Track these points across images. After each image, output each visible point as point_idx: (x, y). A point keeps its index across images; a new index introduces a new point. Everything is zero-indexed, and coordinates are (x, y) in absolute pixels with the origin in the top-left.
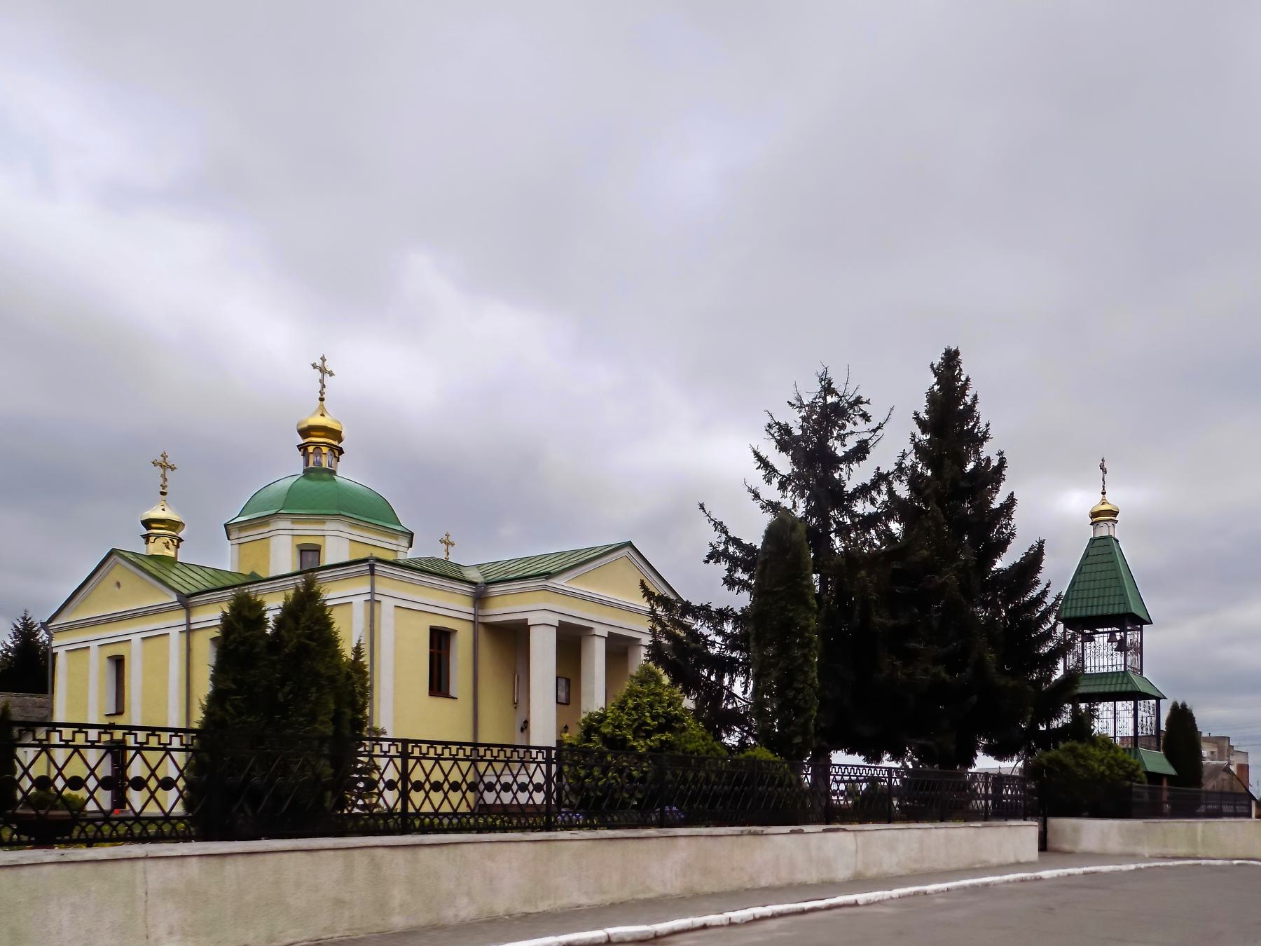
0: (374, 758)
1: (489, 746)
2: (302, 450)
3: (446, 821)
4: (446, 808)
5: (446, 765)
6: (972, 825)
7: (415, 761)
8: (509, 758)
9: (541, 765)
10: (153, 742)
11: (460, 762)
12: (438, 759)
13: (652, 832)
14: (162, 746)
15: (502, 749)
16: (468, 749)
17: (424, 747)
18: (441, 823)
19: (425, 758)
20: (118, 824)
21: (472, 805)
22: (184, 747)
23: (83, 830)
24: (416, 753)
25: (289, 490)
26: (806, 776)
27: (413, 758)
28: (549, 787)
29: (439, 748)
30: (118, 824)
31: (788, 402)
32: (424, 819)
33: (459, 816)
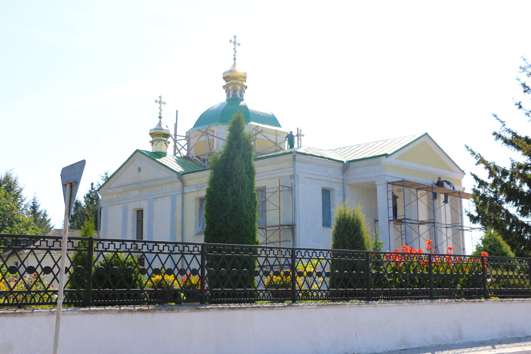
2: (226, 88)
3: (315, 294)
5: (189, 258)
9: (289, 259)
12: (170, 254)
16: (171, 246)
17: (161, 246)
19: (161, 253)
20: (35, 294)
21: (182, 285)
23: (15, 297)
25: (222, 112)
27: (298, 258)
28: (203, 272)
29: (118, 244)
30: (35, 294)
31: (177, 111)
32: (313, 292)
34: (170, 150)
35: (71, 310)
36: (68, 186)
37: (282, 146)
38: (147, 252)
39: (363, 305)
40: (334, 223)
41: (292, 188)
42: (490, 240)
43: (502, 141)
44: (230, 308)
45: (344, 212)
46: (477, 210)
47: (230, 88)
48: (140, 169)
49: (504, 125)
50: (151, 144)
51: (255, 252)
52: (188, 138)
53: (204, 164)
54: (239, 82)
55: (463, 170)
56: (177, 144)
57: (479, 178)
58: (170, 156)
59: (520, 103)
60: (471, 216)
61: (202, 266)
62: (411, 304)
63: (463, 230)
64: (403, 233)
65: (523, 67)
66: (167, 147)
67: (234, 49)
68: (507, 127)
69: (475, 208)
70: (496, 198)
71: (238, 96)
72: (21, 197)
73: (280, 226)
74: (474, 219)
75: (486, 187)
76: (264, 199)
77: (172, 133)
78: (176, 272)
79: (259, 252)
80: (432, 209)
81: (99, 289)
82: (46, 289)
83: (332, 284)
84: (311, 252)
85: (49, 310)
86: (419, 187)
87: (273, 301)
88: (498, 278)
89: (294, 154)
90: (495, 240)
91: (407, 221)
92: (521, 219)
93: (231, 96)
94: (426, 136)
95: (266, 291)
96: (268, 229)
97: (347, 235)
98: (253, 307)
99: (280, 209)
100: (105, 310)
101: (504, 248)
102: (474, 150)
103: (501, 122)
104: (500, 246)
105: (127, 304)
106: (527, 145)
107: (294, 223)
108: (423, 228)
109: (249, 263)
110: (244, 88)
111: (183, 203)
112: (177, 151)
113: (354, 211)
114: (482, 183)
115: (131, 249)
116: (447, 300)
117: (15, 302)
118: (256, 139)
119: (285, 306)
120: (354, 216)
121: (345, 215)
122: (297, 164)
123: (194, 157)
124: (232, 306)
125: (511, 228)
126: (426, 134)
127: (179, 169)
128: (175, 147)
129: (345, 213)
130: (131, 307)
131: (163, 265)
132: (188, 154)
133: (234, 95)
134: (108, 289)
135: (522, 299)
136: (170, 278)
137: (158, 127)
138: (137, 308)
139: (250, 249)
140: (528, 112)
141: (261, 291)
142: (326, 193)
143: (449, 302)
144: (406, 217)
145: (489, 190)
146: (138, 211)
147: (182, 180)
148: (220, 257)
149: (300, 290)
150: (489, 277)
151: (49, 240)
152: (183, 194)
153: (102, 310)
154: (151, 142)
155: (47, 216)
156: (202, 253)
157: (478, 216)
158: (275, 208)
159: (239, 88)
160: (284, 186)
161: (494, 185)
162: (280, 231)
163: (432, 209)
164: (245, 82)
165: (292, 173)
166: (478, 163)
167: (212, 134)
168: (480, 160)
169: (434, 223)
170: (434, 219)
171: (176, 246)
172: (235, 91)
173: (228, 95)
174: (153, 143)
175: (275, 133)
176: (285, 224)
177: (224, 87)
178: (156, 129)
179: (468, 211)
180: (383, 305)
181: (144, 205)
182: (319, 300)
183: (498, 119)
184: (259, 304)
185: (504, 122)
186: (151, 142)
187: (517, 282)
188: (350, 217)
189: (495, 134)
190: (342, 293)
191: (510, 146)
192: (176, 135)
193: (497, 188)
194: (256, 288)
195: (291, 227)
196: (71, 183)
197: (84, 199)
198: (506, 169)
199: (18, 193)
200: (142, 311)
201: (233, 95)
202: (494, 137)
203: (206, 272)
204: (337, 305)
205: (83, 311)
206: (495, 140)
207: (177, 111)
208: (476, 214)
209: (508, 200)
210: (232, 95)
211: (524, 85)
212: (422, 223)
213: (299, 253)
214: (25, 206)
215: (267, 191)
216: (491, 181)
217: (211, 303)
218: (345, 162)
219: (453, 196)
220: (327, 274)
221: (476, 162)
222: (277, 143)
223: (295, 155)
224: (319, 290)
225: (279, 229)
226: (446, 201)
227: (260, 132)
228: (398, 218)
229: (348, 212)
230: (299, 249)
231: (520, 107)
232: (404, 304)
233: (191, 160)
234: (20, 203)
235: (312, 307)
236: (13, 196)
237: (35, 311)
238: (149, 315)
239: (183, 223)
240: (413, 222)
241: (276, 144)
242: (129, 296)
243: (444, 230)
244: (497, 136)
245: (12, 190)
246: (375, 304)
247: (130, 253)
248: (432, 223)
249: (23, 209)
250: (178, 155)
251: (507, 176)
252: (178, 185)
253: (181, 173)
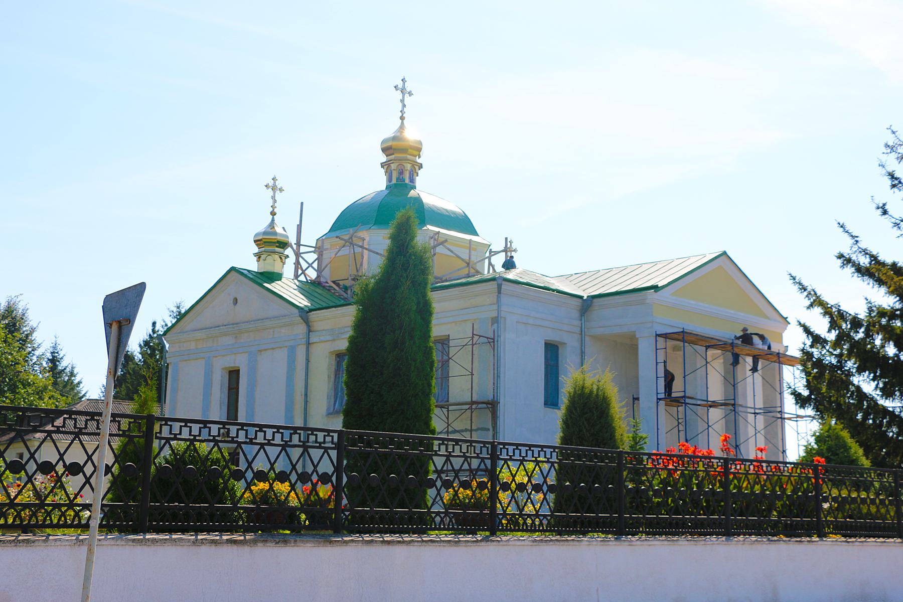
0: (309, 449)
2: (386, 167)
3: (529, 521)
8: (286, 442)
10: (205, 435)
11: (310, 450)
12: (285, 446)
15: (751, 463)
17: (269, 432)
18: (525, 523)
22: (302, 444)
24: (165, 432)
25: (379, 207)
27: (502, 459)
28: (339, 479)
29: (195, 428)
31: (302, 203)
34: (288, 270)
35: (113, 539)
36: (115, 327)
37: (478, 268)
38: (245, 443)
39: (610, 543)
40: (564, 401)
41: (494, 339)
42: (829, 436)
43: (853, 269)
44: (383, 542)
45: (581, 383)
46: (808, 386)
47: (393, 166)
48: (236, 301)
49: (857, 241)
50: (255, 258)
51: (429, 447)
52: (319, 249)
53: (345, 295)
54: (409, 157)
55: (785, 317)
56: (301, 260)
57: (812, 330)
58: (287, 279)
59: (884, 205)
60: (797, 396)
61: (338, 469)
62: (692, 543)
63: (783, 419)
64: (680, 421)
65: (891, 144)
66: (284, 263)
67: (402, 101)
68: (863, 245)
69: (804, 382)
70: (840, 366)
71: (407, 181)
72: (31, 342)
73: (473, 403)
74: (801, 401)
75: (824, 347)
76: (445, 358)
77: (293, 240)
78: (294, 477)
79: (436, 448)
80: (732, 383)
81: (162, 504)
83: (559, 506)
84: (523, 449)
85: (74, 538)
86: (710, 343)
87: (457, 532)
88: (842, 503)
89: (500, 281)
90: (838, 437)
91: (688, 401)
92: (882, 402)
93: (394, 181)
94: (724, 257)
95: (446, 514)
96: (451, 408)
97: (585, 423)
98: (423, 541)
99: (472, 375)
100: (171, 540)
101: (853, 451)
102: (805, 283)
103: (852, 236)
104: (846, 448)
105: (209, 530)
106: (895, 276)
107: (496, 399)
108: (716, 414)
109: (419, 465)
110: (417, 168)
111: (308, 361)
112: (300, 272)
113: (599, 381)
114: (817, 340)
116: (753, 538)
118: (435, 254)
119: (477, 541)
120: (598, 389)
121: (583, 387)
122: (504, 299)
123: (329, 282)
124: (388, 537)
125: (865, 418)
126: (725, 253)
127: (302, 301)
128: (297, 264)
129: (584, 384)
130: (214, 536)
131: (272, 465)
132: (318, 276)
133: (400, 179)
134: (177, 504)
135: (881, 540)
136: (282, 488)
137: (269, 230)
138: (225, 538)
139: (421, 441)
140: (898, 222)
141: (438, 513)
142: (552, 350)
143: (756, 540)
144: (687, 395)
145: (828, 351)
146: (231, 372)
147: (307, 322)
148: (369, 453)
149: (505, 514)
150: (826, 500)
152: (309, 344)
153: (166, 539)
154: (255, 255)
155: (75, 376)
156: (338, 447)
157: (809, 396)
158: (464, 372)
159: (408, 166)
160: (480, 336)
161: (837, 343)
162: (472, 412)
163: (732, 383)
164: (419, 157)
165: (495, 314)
166: (811, 305)
167: (361, 244)
168: (815, 301)
169: (734, 405)
170: (734, 399)
172: (401, 173)
173: (390, 179)
174: (260, 257)
175: (468, 245)
176: (479, 400)
177: (383, 165)
178: (265, 233)
179: (793, 387)
180: (645, 543)
181: (241, 362)
182: (535, 531)
183: (847, 232)
184: (433, 535)
185: (857, 237)
186: (255, 255)
187: (873, 509)
188: (591, 392)
189: (841, 256)
190: (575, 521)
191: (866, 278)
192: (298, 244)
193: (842, 349)
194: (429, 509)
195: (490, 406)
196: (119, 322)
197: (139, 349)
198: (859, 316)
199: (27, 336)
200: (229, 541)
201: (398, 179)
202: (840, 262)
203: (345, 479)
204: (567, 540)
205: (134, 540)
206: (841, 267)
207: (302, 203)
208: (805, 393)
209: (860, 370)
210: (397, 179)
211: (892, 176)
212: (714, 405)
213: (505, 451)
214: (40, 358)
215: (451, 343)
216: (832, 336)
217: (351, 532)
218: (585, 298)
219: (768, 360)
220: (551, 489)
221: (808, 303)
222: (471, 264)
223: (501, 284)
224: (537, 515)
225: (471, 408)
226: (754, 369)
227: (442, 243)
228: (674, 395)
229: (588, 383)
230: (504, 444)
231: (885, 212)
232: (680, 543)
233: (324, 287)
234: (30, 353)
235: (523, 543)
236: (18, 341)
237: (51, 538)
238: (246, 549)
239: (306, 395)
240: (699, 402)
241: (468, 264)
242: (212, 518)
243: (751, 417)
244: (845, 260)
245: (18, 330)
246: (632, 541)
248: (731, 405)
249: (34, 364)
250: (302, 278)
251: (860, 328)
252: (301, 328)
253: (307, 309)
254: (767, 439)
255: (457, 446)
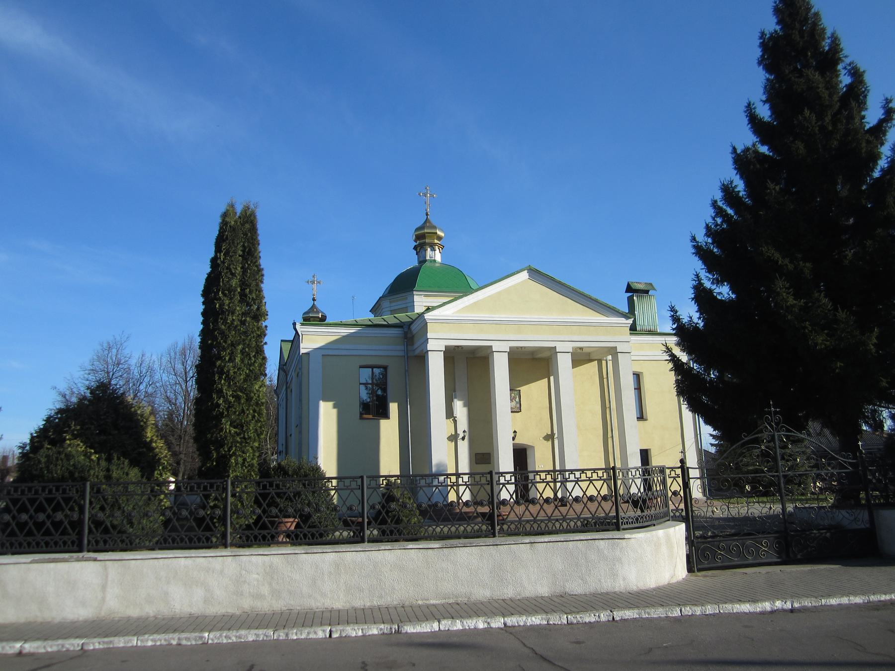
1: (572, 471)
3: (572, 524)
4: (528, 517)
6: (383, 548)
7: (560, 484)
8: (578, 478)
10: (583, 477)
12: (577, 481)
13: (66, 555)
14: (464, 483)
24: (502, 480)
26: (633, 481)
27: (434, 486)
29: (578, 474)
33: (568, 521)
38: (425, 486)
79: (513, 478)
82: (535, 519)
115: (469, 482)
117: (561, 528)
131: (599, 492)
151: (346, 480)
171: (447, 478)
247: (591, 481)
254: (157, 631)
255: (340, 483)
